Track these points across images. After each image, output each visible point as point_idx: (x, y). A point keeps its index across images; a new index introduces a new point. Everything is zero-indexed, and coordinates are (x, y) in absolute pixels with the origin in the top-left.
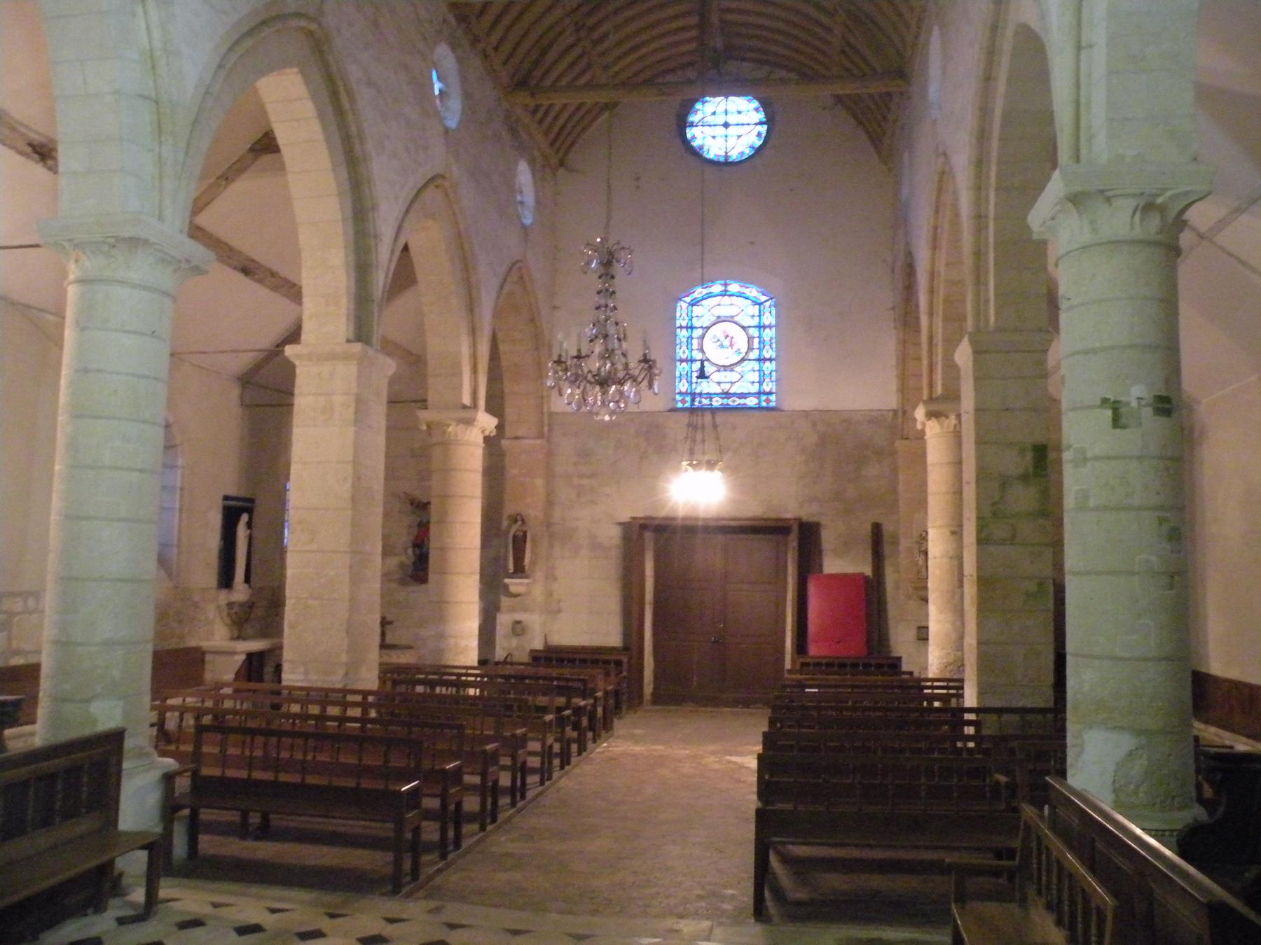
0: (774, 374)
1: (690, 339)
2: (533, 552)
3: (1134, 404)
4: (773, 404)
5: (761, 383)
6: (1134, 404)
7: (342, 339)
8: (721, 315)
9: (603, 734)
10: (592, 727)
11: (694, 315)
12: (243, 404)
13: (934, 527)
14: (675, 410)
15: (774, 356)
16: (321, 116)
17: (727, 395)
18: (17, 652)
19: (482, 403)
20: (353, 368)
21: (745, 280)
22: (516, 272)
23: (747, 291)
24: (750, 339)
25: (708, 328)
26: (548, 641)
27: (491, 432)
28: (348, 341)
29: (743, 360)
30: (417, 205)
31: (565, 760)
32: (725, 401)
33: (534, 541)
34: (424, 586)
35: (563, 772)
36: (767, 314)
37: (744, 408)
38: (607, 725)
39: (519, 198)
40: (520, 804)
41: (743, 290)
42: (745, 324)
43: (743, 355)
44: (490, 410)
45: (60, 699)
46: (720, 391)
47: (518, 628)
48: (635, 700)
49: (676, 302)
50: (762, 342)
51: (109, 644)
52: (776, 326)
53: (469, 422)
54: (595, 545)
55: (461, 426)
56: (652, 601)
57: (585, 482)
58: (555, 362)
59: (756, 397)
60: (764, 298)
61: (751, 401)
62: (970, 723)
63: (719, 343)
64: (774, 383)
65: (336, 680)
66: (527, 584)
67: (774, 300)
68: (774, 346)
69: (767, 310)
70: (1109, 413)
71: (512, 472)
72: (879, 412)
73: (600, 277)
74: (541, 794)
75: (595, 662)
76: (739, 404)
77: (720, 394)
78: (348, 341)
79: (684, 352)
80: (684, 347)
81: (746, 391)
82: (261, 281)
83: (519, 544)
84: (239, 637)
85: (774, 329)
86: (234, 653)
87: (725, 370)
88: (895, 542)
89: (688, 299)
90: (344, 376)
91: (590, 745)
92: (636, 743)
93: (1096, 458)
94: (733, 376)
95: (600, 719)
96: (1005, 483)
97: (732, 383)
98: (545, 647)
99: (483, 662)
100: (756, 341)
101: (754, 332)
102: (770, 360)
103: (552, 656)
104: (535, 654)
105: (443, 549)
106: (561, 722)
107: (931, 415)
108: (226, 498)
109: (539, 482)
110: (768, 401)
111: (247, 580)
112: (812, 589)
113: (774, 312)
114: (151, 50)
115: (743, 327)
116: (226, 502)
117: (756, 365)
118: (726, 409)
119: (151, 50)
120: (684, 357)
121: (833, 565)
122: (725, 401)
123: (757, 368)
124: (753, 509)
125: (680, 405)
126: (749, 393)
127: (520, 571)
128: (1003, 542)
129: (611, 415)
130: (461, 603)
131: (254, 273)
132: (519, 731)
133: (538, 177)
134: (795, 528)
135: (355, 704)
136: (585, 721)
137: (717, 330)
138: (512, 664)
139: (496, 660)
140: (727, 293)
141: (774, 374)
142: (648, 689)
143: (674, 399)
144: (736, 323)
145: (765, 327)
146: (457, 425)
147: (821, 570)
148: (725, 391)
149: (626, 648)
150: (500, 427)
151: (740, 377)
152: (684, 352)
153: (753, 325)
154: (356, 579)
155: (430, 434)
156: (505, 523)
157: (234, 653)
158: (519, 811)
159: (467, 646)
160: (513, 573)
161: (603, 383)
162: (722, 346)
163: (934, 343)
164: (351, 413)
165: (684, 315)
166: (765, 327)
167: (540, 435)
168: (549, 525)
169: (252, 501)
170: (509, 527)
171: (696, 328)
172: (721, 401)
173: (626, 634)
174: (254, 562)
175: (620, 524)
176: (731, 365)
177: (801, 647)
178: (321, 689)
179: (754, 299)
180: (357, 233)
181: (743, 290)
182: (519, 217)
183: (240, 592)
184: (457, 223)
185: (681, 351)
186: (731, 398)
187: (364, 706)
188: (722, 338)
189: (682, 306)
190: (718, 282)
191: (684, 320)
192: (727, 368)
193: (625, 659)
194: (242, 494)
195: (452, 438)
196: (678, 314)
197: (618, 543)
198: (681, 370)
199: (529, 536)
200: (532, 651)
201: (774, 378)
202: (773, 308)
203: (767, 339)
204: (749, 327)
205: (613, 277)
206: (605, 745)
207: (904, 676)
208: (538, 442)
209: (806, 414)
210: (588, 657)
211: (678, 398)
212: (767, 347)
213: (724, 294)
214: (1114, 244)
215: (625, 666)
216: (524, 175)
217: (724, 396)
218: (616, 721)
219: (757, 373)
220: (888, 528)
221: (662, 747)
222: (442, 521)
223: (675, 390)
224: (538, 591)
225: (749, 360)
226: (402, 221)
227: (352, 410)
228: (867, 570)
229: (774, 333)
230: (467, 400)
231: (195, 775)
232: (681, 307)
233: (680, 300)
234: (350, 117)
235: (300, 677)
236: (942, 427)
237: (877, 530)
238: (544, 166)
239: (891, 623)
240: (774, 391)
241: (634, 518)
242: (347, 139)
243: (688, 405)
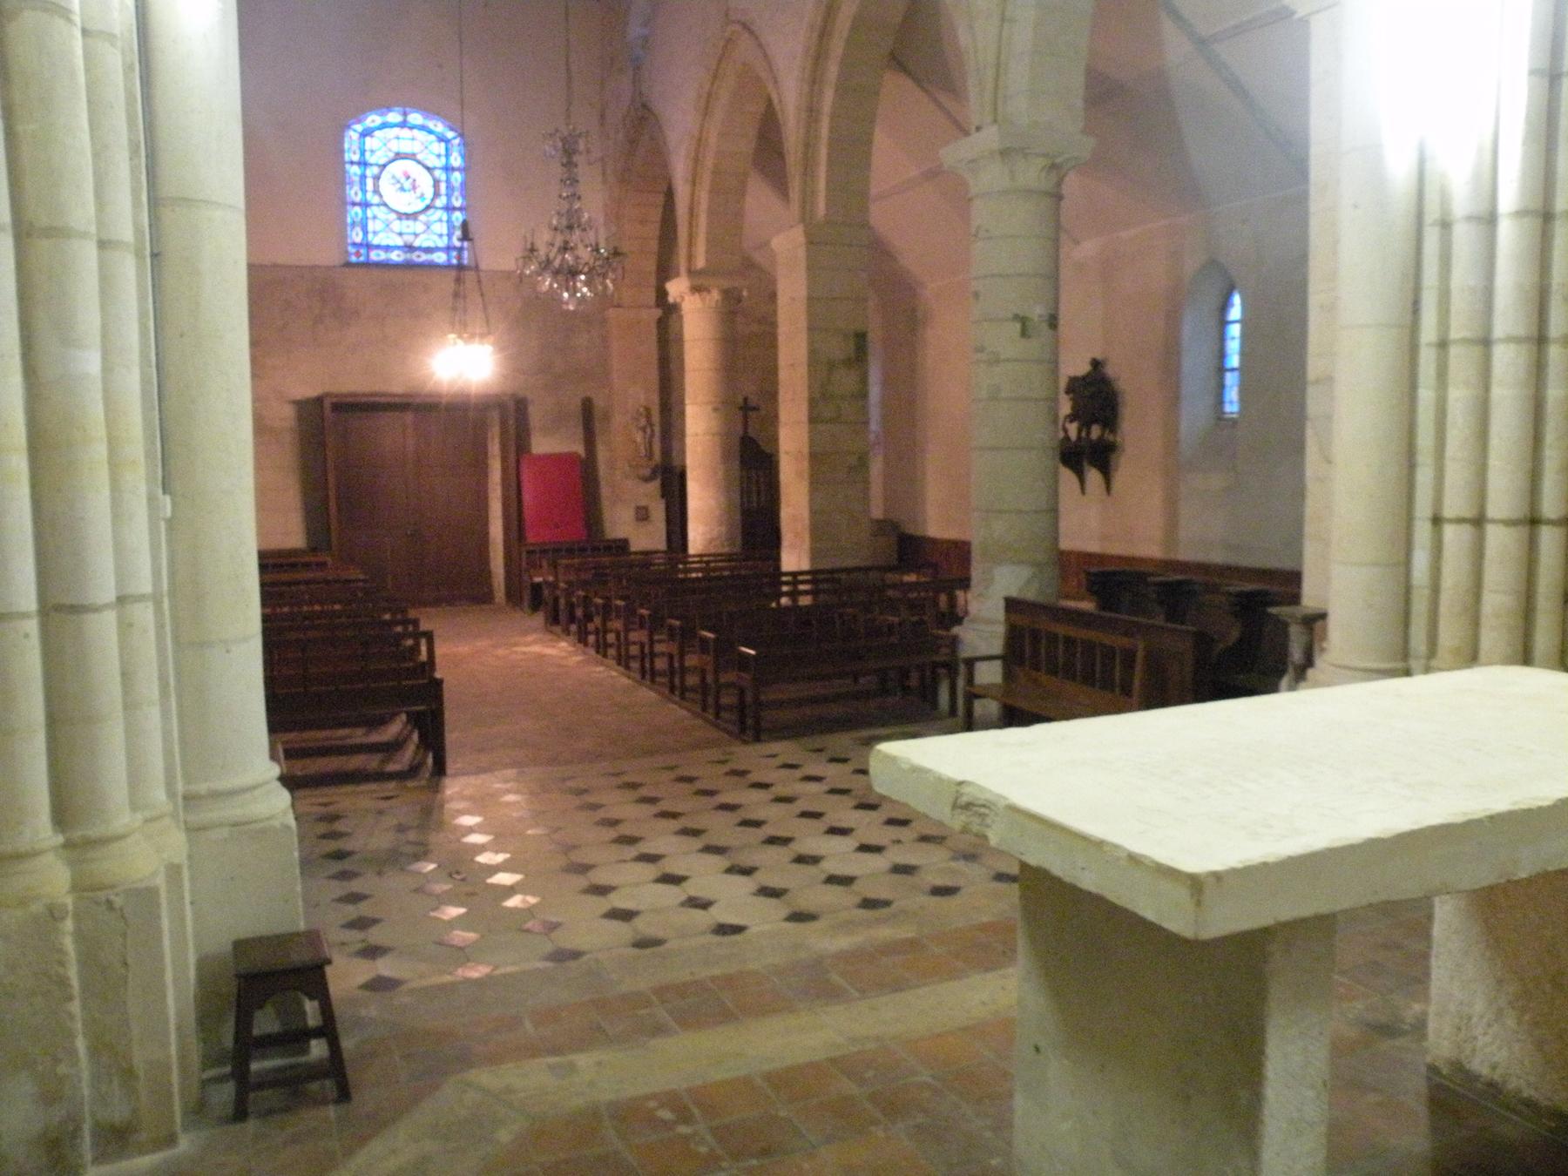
3: (1036, 319)
6: (1036, 319)
13: (692, 404)
14: (348, 265)
17: (409, 248)
21: (429, 111)
24: (436, 183)
25: (384, 166)
29: (428, 208)
32: (408, 256)
37: (432, 266)
43: (428, 202)
49: (343, 131)
50: (450, 187)
62: (786, 583)
70: (1018, 326)
81: (432, 245)
88: (607, 417)
89: (359, 128)
93: (1008, 360)
94: (418, 227)
96: (831, 366)
107: (696, 289)
115: (428, 169)
118: (408, 266)
121: (542, 445)
122: (408, 256)
125: (354, 259)
128: (831, 421)
137: (398, 168)
143: (347, 252)
144: (419, 162)
162: (402, 189)
163: (695, 214)
189: (352, 135)
196: (346, 146)
207: (632, 557)
211: (352, 250)
214: (1029, 192)
220: (599, 403)
228: (579, 448)
232: (351, 137)
236: (703, 300)
237: (587, 408)
239: (605, 504)
243: (362, 259)
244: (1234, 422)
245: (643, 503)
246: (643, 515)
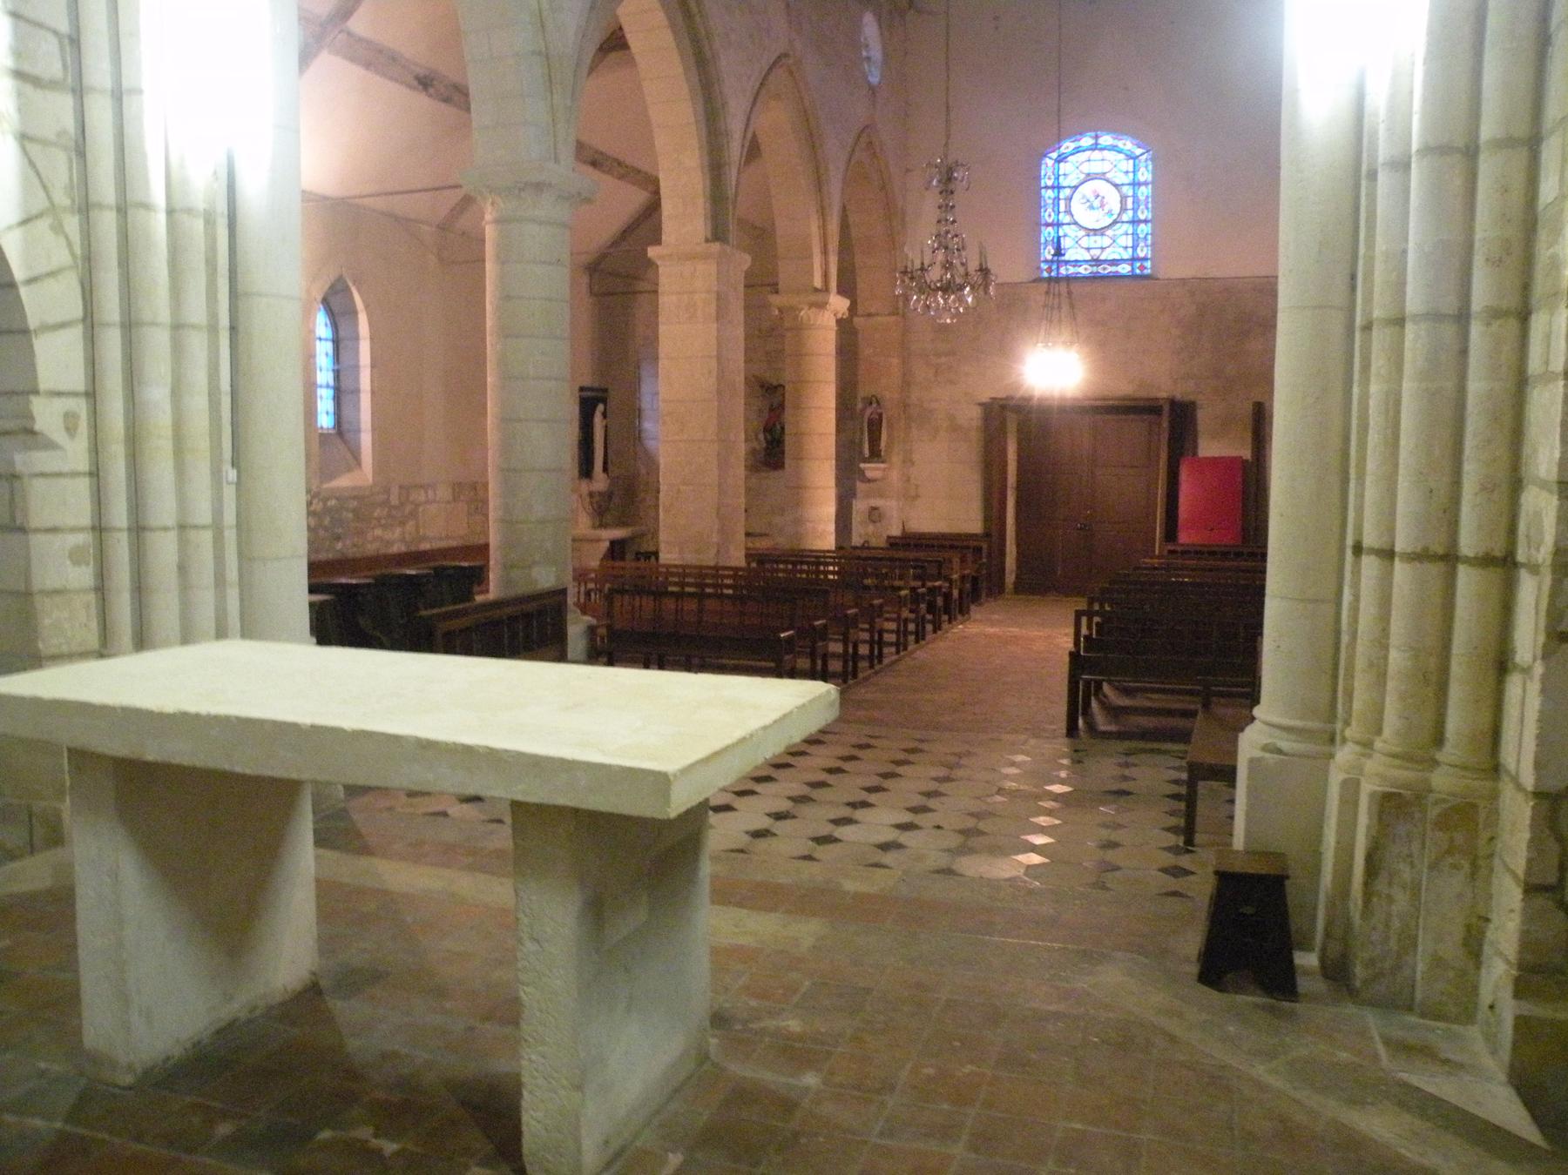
0: (1149, 237)
1: (1056, 201)
2: (889, 436)
4: (1148, 272)
5: (1134, 248)
7: (701, 237)
8: (1091, 171)
9: (959, 617)
10: (947, 610)
11: (1061, 173)
12: (591, 293)
14: (1040, 280)
15: (1150, 217)
16: (673, 26)
17: (1096, 262)
18: (424, 538)
19: (833, 284)
20: (713, 268)
21: (1117, 131)
22: (866, 138)
23: (1120, 144)
24: (1123, 198)
25: (1076, 187)
26: (906, 530)
27: (843, 314)
28: (707, 241)
29: (1115, 222)
30: (763, 91)
31: (920, 636)
32: (1095, 269)
33: (890, 426)
34: (776, 474)
35: (918, 645)
36: (1143, 170)
37: (1118, 277)
38: (964, 611)
39: (864, 54)
40: (877, 667)
41: (1116, 142)
42: (1118, 181)
43: (1115, 217)
44: (842, 291)
45: (508, 567)
46: (1089, 258)
47: (874, 514)
48: (997, 589)
50: (1136, 201)
51: (542, 522)
52: (1152, 183)
53: (822, 306)
54: (955, 428)
55: (814, 309)
56: (1015, 485)
57: (943, 360)
58: (902, 272)
59: (1128, 264)
60: (1139, 151)
61: (1124, 268)
63: (1088, 204)
64: (1149, 248)
65: (709, 559)
66: (884, 470)
67: (1151, 152)
68: (1150, 205)
69: (1143, 164)
71: (866, 351)
72: (1266, 279)
73: (941, 193)
74: (897, 661)
75: (952, 547)
76: (1110, 272)
77: (1090, 261)
78: (707, 241)
79: (1050, 216)
80: (1049, 210)
81: (1118, 257)
82: (609, 172)
83: (875, 426)
84: (603, 526)
85: (1150, 186)
86: (598, 540)
87: (1095, 235)
89: (1054, 155)
90: (703, 277)
91: (945, 626)
92: (992, 625)
94: (1105, 241)
95: (955, 601)
97: (1103, 249)
98: (902, 534)
99: (839, 548)
100: (1130, 201)
101: (1128, 191)
102: (1146, 221)
103: (910, 542)
104: (892, 541)
105: (799, 435)
106: (915, 597)
108: (582, 389)
109: (895, 361)
110: (1142, 268)
111: (605, 469)
112: (1184, 475)
113: (1150, 167)
114: (540, 11)
116: (582, 393)
117: (1130, 229)
118: (1094, 278)
119: (540, 11)
120: (1050, 221)
121: (1209, 448)
122: (1095, 269)
123: (1130, 231)
124: (1123, 387)
125: (1045, 274)
126: (1122, 260)
127: (875, 455)
129: (952, 319)
130: (818, 488)
131: (601, 165)
132: (876, 602)
133: (886, 27)
134: (1166, 408)
135: (728, 577)
136: (940, 601)
138: (868, 548)
139: (853, 544)
140: (1099, 147)
141: (1149, 237)
142: (1010, 578)
143: (1039, 268)
144: (1108, 181)
145: (1140, 184)
146: (809, 309)
147: (1195, 454)
148: (1095, 258)
149: (987, 535)
150: (853, 309)
151: (1111, 241)
152: (1050, 216)
153: (1127, 182)
154: (723, 464)
155: (781, 318)
156: (860, 406)
157: (598, 540)
158: (876, 673)
159: (824, 531)
160: (870, 456)
161: (946, 289)
162: (1091, 207)
164: (712, 309)
165: (1050, 173)
166: (1140, 184)
167: (894, 313)
168: (906, 406)
169: (606, 390)
170: (863, 410)
171: (1064, 187)
172: (1090, 269)
173: (987, 519)
174: (611, 455)
175: (980, 404)
176: (1102, 228)
177: (1171, 534)
178: (696, 567)
179: (1128, 153)
180: (709, 133)
181: (1116, 142)
182: (865, 78)
183: (600, 482)
184: (802, 98)
185: (1047, 214)
186: (1100, 265)
187: (734, 577)
188: (1092, 199)
190: (1088, 134)
191: (1049, 178)
192: (1097, 232)
193: (985, 546)
194: (596, 385)
195: (804, 321)
196: (1043, 173)
197: (979, 424)
198: (1046, 235)
199: (884, 416)
200: (889, 537)
201: (1149, 242)
202: (1150, 163)
203: (1142, 198)
204: (1123, 185)
205: (952, 192)
206: (961, 626)
208: (893, 318)
209: (1183, 281)
210: (947, 543)
211: (1044, 266)
212: (1142, 207)
213: (1095, 147)
215: (985, 552)
216: (870, 28)
217: (1093, 263)
218: (973, 607)
219: (1130, 237)
221: (1017, 630)
222: (797, 407)
223: (1040, 257)
224: (895, 476)
225: (1123, 222)
226: (751, 112)
227: (714, 306)
228: (1246, 453)
229: (1150, 191)
230: (818, 283)
231: (609, 627)
232: (1046, 164)
233: (1045, 156)
234: (698, 19)
235: (675, 556)
238: (890, 12)
240: (1149, 256)
241: (994, 399)
242: (696, 41)
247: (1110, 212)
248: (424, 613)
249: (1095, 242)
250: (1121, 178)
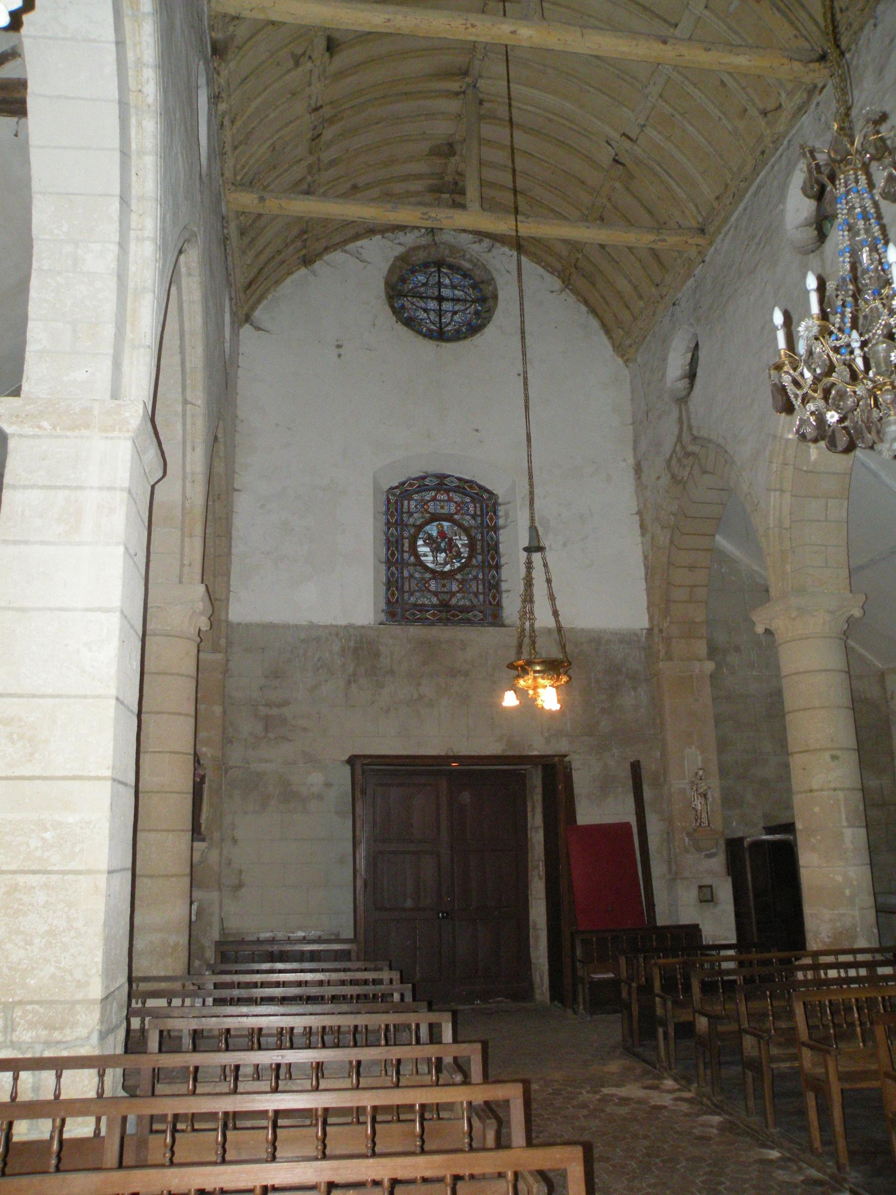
61: (475, 616)
244: (104, 1137)
245: (707, 882)
246: (707, 896)
247: (458, 555)
248: (569, 728)
249: (442, 507)
250: (468, 521)
